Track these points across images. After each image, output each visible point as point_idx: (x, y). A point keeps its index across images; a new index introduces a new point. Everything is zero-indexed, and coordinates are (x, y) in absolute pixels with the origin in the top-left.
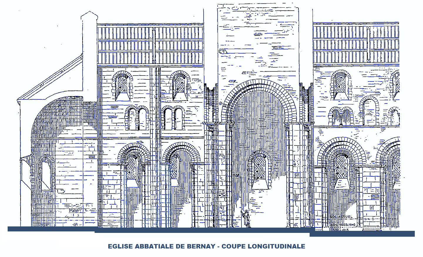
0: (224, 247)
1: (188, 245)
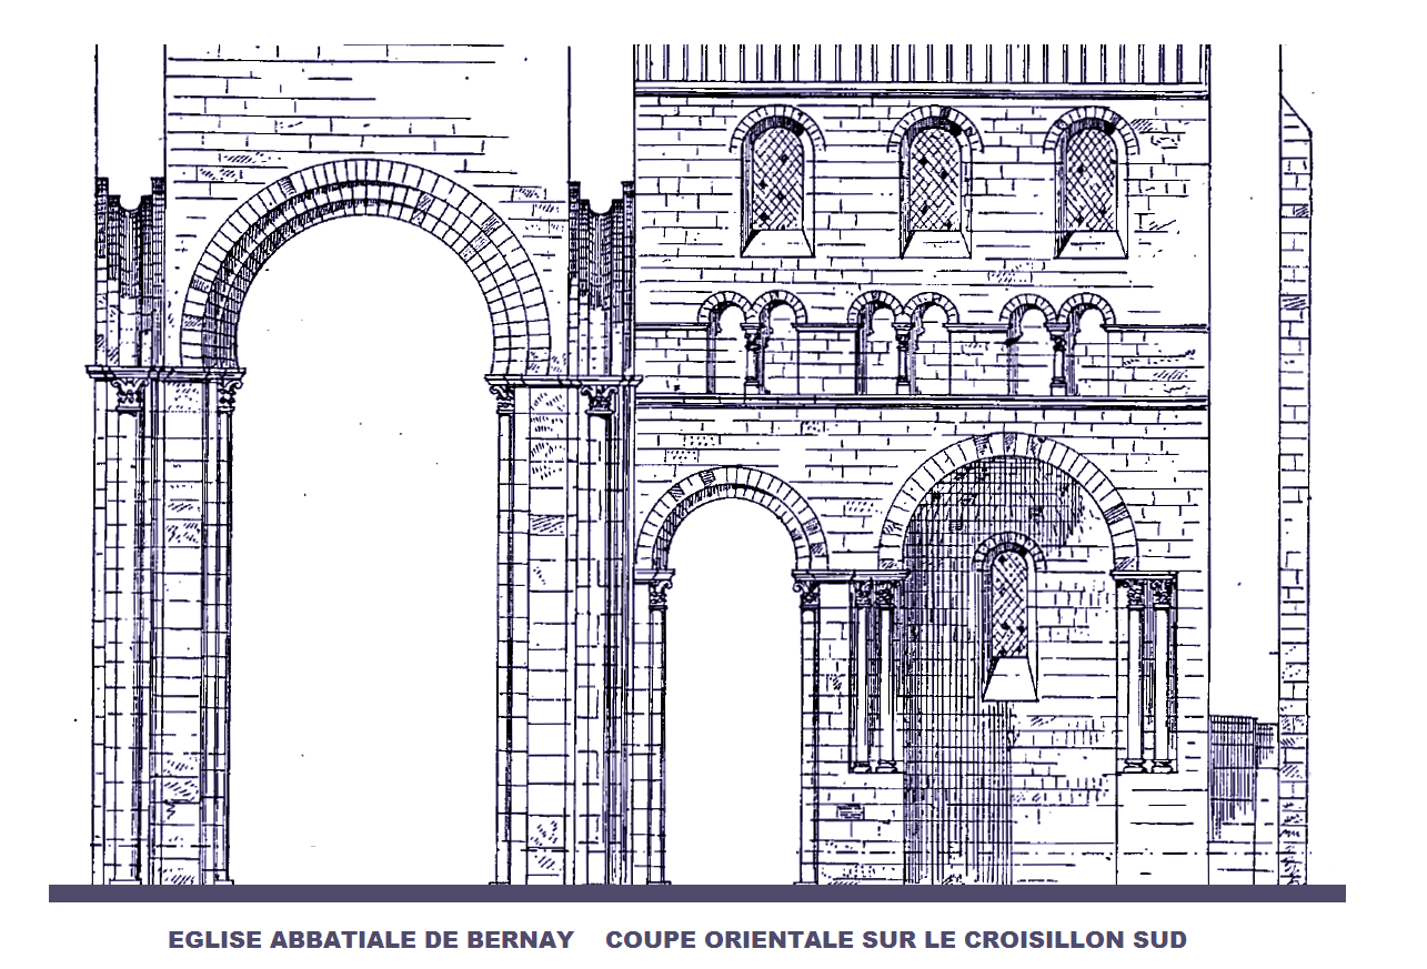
1: (471, 934)
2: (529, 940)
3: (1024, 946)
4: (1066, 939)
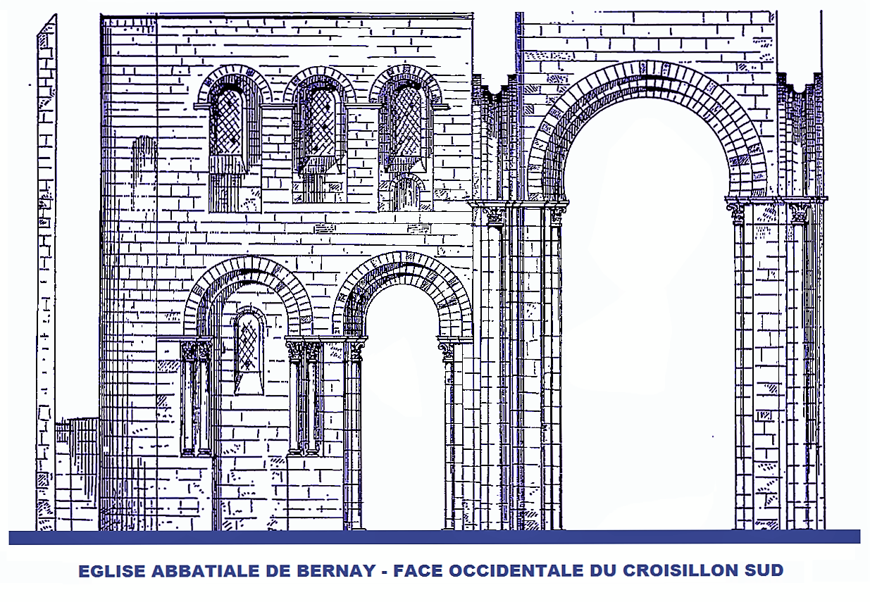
0: (96, 573)
1: (300, 567)
2: (342, 571)
3: (667, 575)
4: (697, 570)
